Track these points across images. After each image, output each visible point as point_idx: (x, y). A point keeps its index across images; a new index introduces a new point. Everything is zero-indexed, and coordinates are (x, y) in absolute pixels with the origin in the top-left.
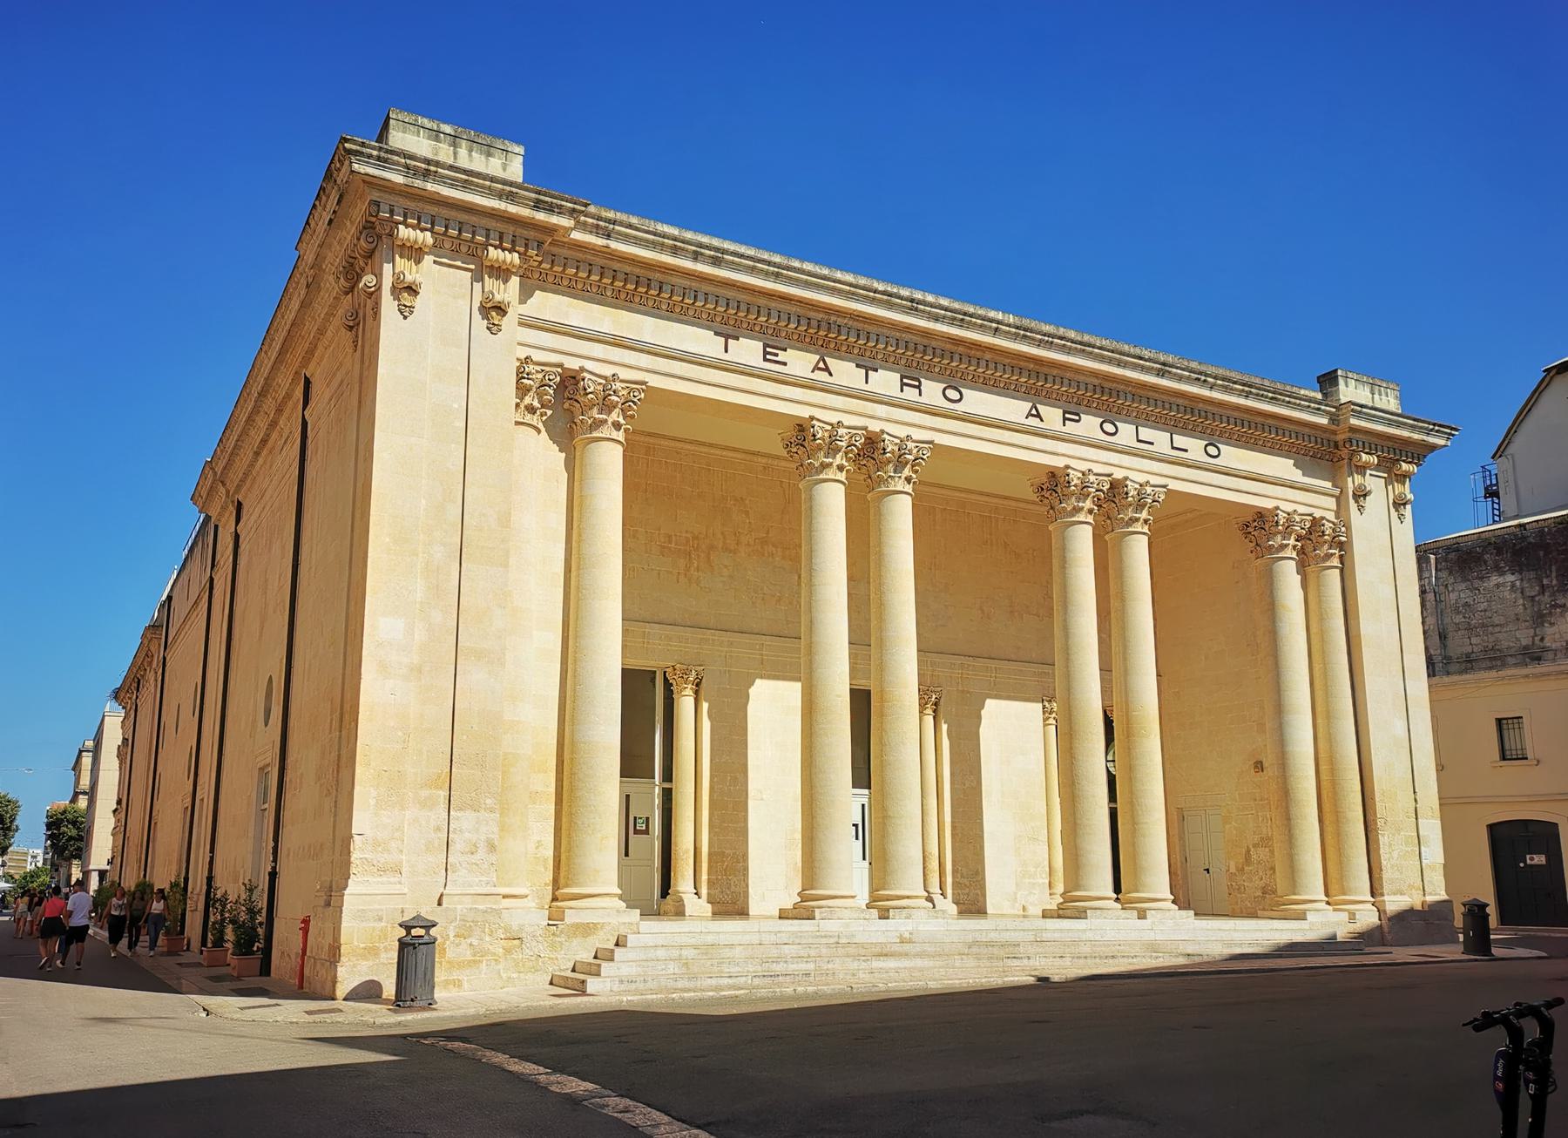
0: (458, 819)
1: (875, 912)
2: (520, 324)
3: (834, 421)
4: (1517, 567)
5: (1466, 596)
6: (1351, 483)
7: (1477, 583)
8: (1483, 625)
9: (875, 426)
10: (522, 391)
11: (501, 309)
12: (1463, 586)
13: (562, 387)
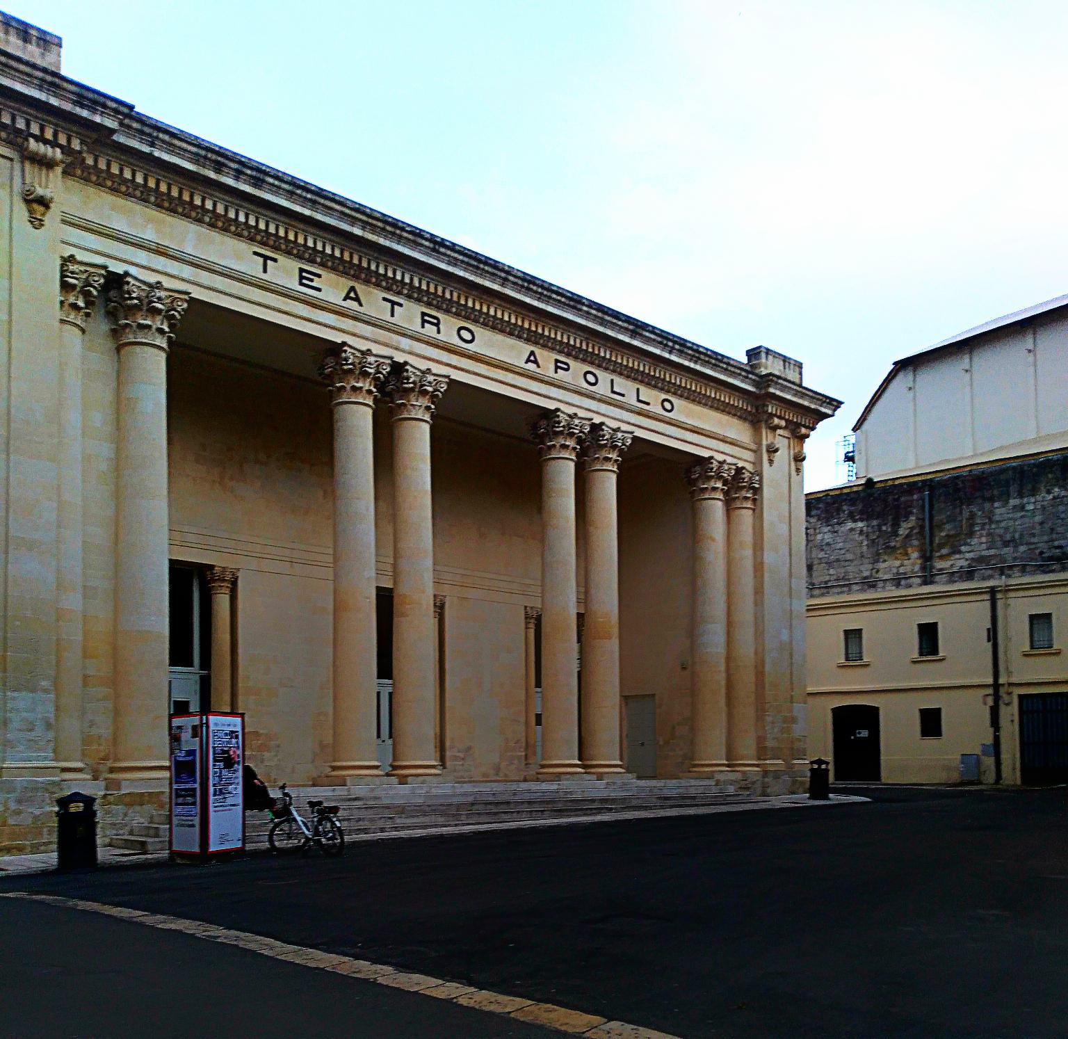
0: (14, 699)
1: (394, 780)
2: (64, 222)
3: (364, 349)
4: (866, 515)
5: (828, 538)
6: (767, 438)
7: (837, 528)
8: (838, 560)
9: (400, 358)
10: (66, 287)
11: (44, 203)
12: (826, 529)
13: (105, 289)
